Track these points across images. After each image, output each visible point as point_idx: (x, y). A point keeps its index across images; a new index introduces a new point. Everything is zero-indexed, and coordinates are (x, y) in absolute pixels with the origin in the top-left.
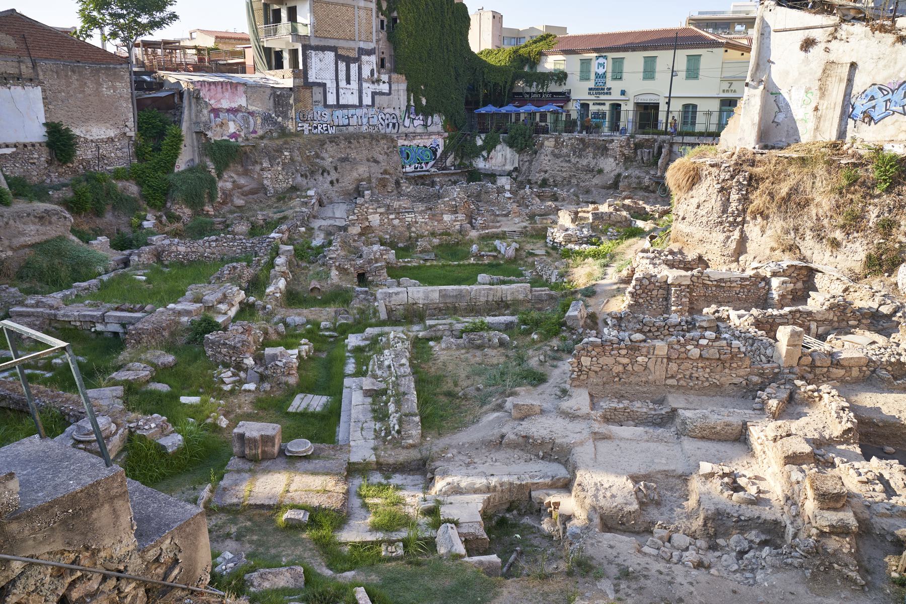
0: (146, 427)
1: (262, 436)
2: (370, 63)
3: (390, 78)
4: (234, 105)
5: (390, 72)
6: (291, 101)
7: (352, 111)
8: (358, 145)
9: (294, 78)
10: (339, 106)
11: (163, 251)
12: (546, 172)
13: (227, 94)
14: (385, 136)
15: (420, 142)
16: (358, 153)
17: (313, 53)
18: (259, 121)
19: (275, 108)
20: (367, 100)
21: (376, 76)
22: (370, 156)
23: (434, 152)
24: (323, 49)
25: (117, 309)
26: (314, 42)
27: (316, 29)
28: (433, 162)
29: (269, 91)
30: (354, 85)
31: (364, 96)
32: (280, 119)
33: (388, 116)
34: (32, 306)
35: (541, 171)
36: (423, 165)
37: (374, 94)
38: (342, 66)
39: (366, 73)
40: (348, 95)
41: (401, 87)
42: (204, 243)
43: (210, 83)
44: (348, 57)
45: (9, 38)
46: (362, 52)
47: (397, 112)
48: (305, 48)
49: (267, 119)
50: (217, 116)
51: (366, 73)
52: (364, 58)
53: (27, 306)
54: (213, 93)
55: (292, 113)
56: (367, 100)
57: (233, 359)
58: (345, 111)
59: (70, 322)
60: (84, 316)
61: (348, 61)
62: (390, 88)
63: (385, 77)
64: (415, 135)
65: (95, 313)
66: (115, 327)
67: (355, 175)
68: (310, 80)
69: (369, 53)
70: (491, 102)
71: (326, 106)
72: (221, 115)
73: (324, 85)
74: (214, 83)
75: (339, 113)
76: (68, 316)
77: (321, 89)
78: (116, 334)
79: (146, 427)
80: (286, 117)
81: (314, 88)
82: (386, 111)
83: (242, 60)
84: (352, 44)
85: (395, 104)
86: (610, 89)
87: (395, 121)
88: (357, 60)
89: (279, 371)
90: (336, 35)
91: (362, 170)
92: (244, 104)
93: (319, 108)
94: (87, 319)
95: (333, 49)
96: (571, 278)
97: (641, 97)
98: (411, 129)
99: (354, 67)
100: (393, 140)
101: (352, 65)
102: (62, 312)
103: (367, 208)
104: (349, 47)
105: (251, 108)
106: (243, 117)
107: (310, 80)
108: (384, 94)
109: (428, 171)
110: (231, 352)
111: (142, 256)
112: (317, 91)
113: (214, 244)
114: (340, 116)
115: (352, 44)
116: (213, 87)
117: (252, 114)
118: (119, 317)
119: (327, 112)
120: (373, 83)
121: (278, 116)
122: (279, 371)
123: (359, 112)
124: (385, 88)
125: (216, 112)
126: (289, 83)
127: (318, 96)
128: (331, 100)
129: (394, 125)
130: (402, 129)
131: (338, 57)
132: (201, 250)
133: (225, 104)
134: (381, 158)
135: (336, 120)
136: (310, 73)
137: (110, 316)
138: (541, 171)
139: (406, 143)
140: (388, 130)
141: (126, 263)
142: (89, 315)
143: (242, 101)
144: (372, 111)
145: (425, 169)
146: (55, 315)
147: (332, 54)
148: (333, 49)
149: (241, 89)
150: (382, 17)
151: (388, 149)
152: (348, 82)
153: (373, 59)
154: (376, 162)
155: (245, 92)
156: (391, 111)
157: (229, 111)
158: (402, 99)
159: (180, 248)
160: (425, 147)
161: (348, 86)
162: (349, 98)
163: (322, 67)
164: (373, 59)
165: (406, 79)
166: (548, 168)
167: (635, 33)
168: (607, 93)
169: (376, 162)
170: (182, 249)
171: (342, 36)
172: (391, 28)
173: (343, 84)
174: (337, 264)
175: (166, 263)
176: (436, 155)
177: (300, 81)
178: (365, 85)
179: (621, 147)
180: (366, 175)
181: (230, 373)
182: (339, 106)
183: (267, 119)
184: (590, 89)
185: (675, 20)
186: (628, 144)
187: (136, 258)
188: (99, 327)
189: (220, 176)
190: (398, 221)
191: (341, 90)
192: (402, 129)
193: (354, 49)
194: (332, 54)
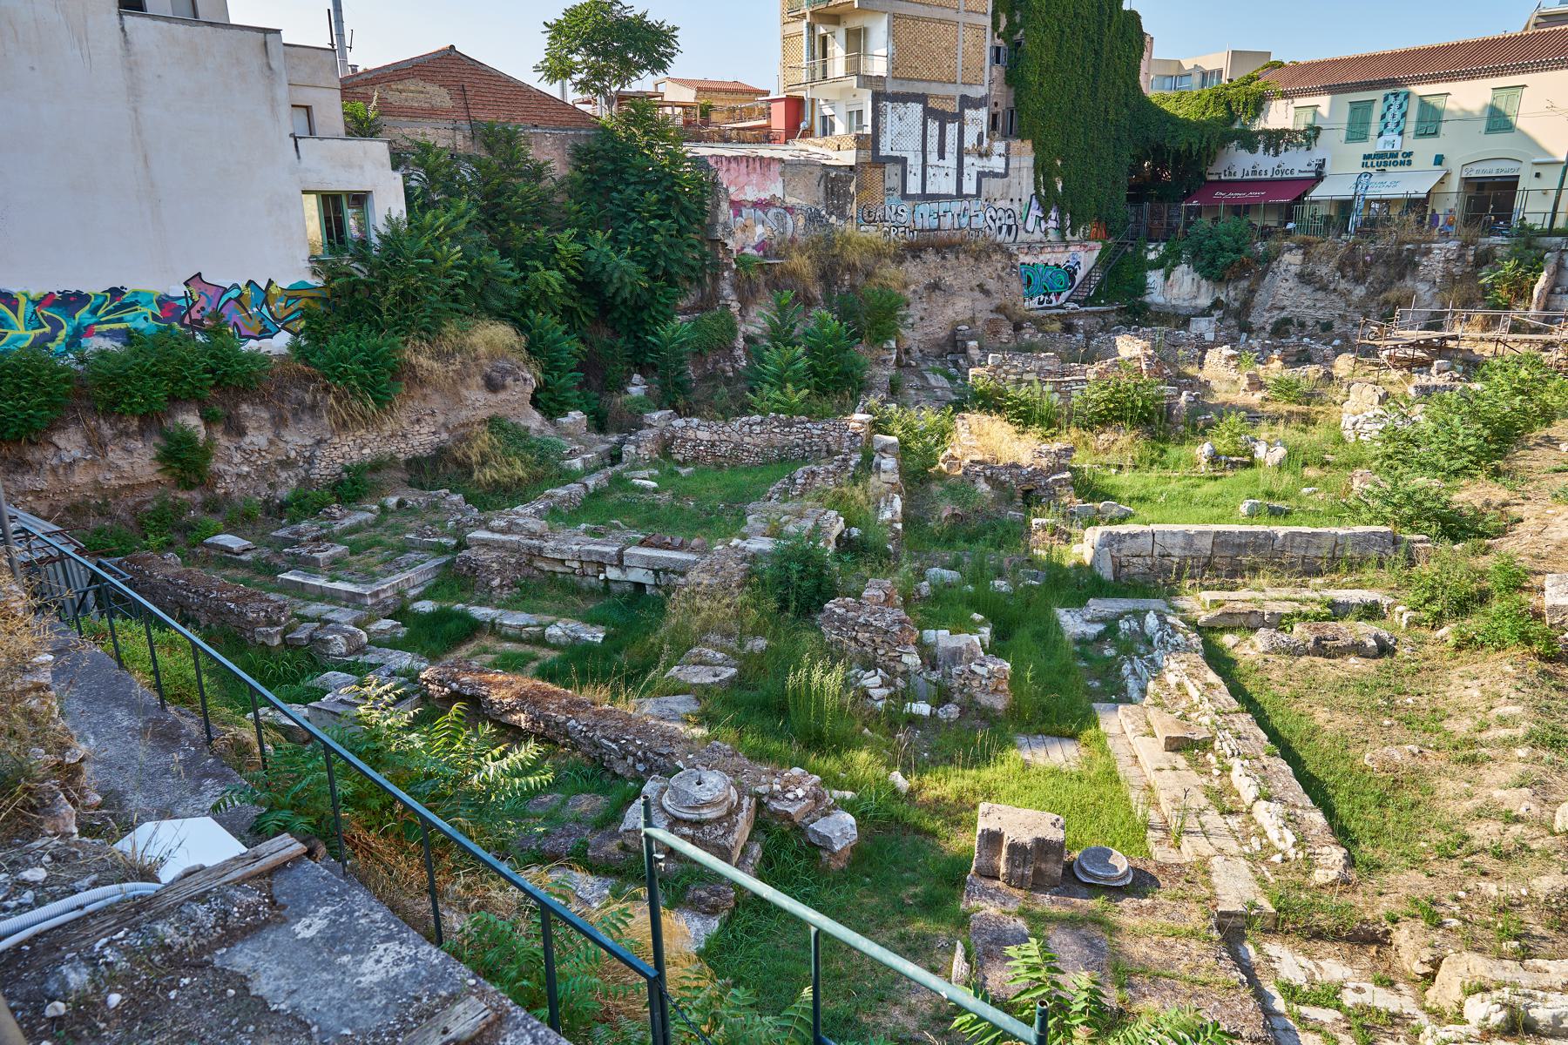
0: (790, 796)
1: (1038, 840)
2: (977, 120)
3: (1008, 148)
4: (765, 195)
5: (1004, 137)
6: (852, 189)
7: (945, 205)
8: (954, 261)
9: (858, 149)
10: (925, 197)
11: (674, 438)
12: (1283, 308)
13: (754, 178)
14: (999, 248)
15: (1049, 257)
16: (959, 273)
17: (890, 105)
18: (801, 222)
19: (826, 199)
20: (969, 187)
21: (985, 145)
22: (975, 283)
23: (1071, 274)
24: (905, 98)
25: (642, 543)
26: (891, 88)
27: (895, 64)
28: (1068, 293)
29: (818, 172)
30: (951, 160)
31: (966, 178)
32: (833, 219)
33: (1000, 213)
34: (502, 532)
35: (1273, 307)
36: (1053, 297)
37: (981, 175)
38: (934, 127)
39: (970, 140)
40: (941, 178)
41: (1024, 157)
42: (741, 427)
43: (729, 159)
44: (943, 112)
45: (444, 91)
46: (966, 102)
47: (1016, 206)
48: (877, 98)
49: (813, 218)
50: (738, 213)
51: (970, 140)
52: (969, 113)
53: (493, 530)
54: (733, 173)
55: (852, 209)
56: (969, 187)
57: (881, 652)
58: (934, 206)
59: (563, 561)
60: (589, 552)
61: (943, 118)
62: (1007, 164)
63: (999, 147)
64: (1043, 246)
65: (607, 549)
66: (638, 575)
67: (950, 312)
68: (883, 153)
69: (976, 104)
70: (1159, 191)
71: (905, 196)
72: (745, 212)
73: (903, 161)
74: (735, 158)
75: (924, 208)
76: (562, 552)
77: (899, 167)
78: (640, 586)
79: (790, 796)
80: (842, 215)
81: (888, 166)
82: (998, 204)
83: (764, 122)
84: (951, 90)
85: (1013, 193)
86: (1410, 154)
87: (1011, 222)
88: (959, 117)
89: (975, 683)
90: (926, 74)
91: (961, 307)
92: (779, 194)
93: (894, 200)
94: (594, 558)
95: (922, 98)
96: (290, 421)
97: (1476, 167)
98: (1038, 236)
99: (952, 129)
100: (1011, 256)
101: (949, 127)
102: (552, 544)
103: (1007, 372)
104: (946, 94)
105: (790, 201)
106: (777, 215)
107: (883, 153)
108: (996, 175)
109: (1060, 307)
110: (878, 640)
111: (640, 446)
112: (893, 169)
113: (757, 429)
114: (925, 215)
115: (951, 90)
116: (733, 165)
117: (790, 210)
118: (649, 558)
119: (906, 206)
120: (981, 155)
121: (831, 214)
122: (975, 683)
123: (957, 206)
124: (997, 164)
125: (737, 206)
126: (848, 158)
127: (894, 181)
128: (914, 187)
129: (1009, 227)
130: (1022, 236)
131: (929, 113)
132: (735, 437)
133: (751, 195)
134: (992, 285)
135: (919, 220)
136: (882, 140)
137: (632, 556)
138: (1273, 307)
139: (1027, 259)
140: (1000, 238)
141: (615, 457)
142: (597, 552)
143: (775, 189)
144: (975, 206)
145: (1054, 303)
146: (540, 549)
147: (919, 107)
148: (922, 98)
149: (776, 168)
150: (999, 42)
151: (1003, 269)
152: (942, 156)
153: (983, 114)
154: (987, 293)
155: (782, 174)
156: (1005, 204)
157: (757, 205)
158: (1024, 183)
159: (700, 435)
160: (1058, 266)
161: (941, 163)
162: (943, 184)
163: (903, 130)
164: (983, 114)
165: (1034, 148)
166: (1286, 303)
167: (1466, 45)
168: (1402, 163)
169: (987, 293)
170: (704, 435)
171: (936, 75)
172: (1011, 59)
173: (933, 158)
174: (988, 472)
175: (680, 457)
176: (1073, 281)
177: (867, 155)
178: (967, 160)
179: (1447, 261)
180: (968, 314)
181: (877, 680)
182: (925, 197)
183: (813, 218)
184: (1366, 157)
185: (1515, 24)
186: (1461, 257)
187: (632, 449)
188: (613, 573)
189: (743, 310)
190: (1057, 395)
191: (929, 169)
192: (1022, 236)
193: (953, 99)
194: (919, 107)
